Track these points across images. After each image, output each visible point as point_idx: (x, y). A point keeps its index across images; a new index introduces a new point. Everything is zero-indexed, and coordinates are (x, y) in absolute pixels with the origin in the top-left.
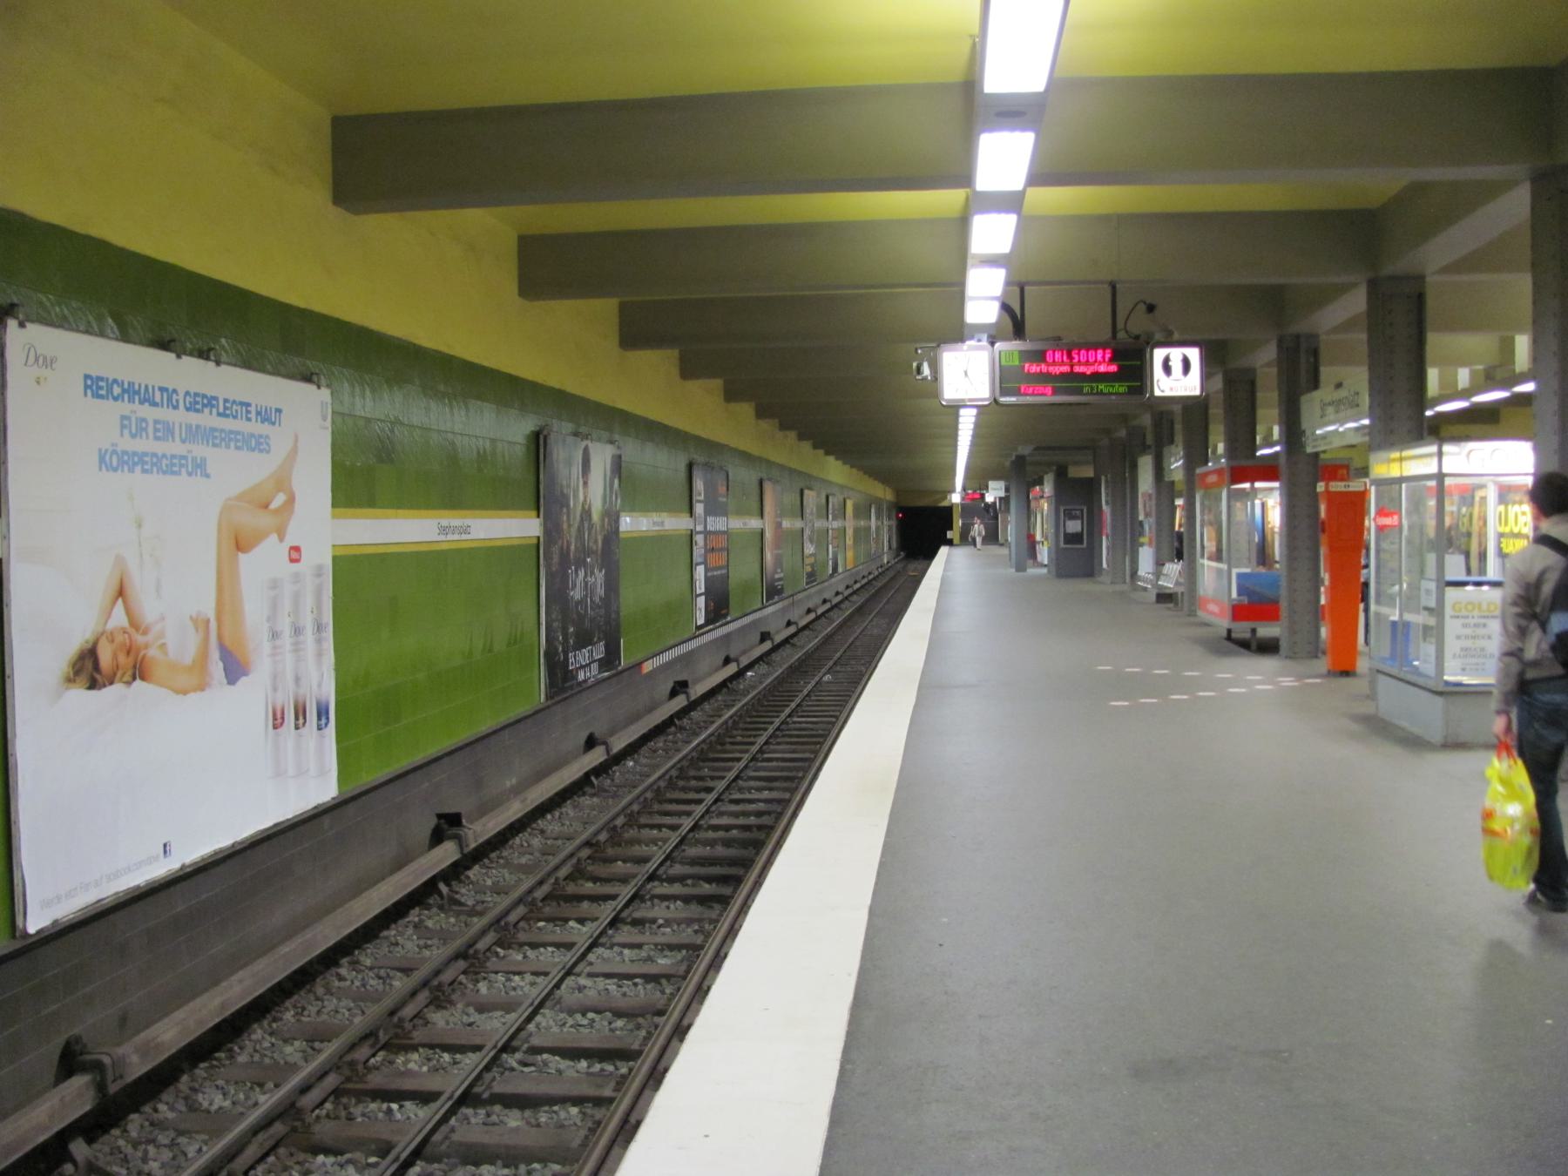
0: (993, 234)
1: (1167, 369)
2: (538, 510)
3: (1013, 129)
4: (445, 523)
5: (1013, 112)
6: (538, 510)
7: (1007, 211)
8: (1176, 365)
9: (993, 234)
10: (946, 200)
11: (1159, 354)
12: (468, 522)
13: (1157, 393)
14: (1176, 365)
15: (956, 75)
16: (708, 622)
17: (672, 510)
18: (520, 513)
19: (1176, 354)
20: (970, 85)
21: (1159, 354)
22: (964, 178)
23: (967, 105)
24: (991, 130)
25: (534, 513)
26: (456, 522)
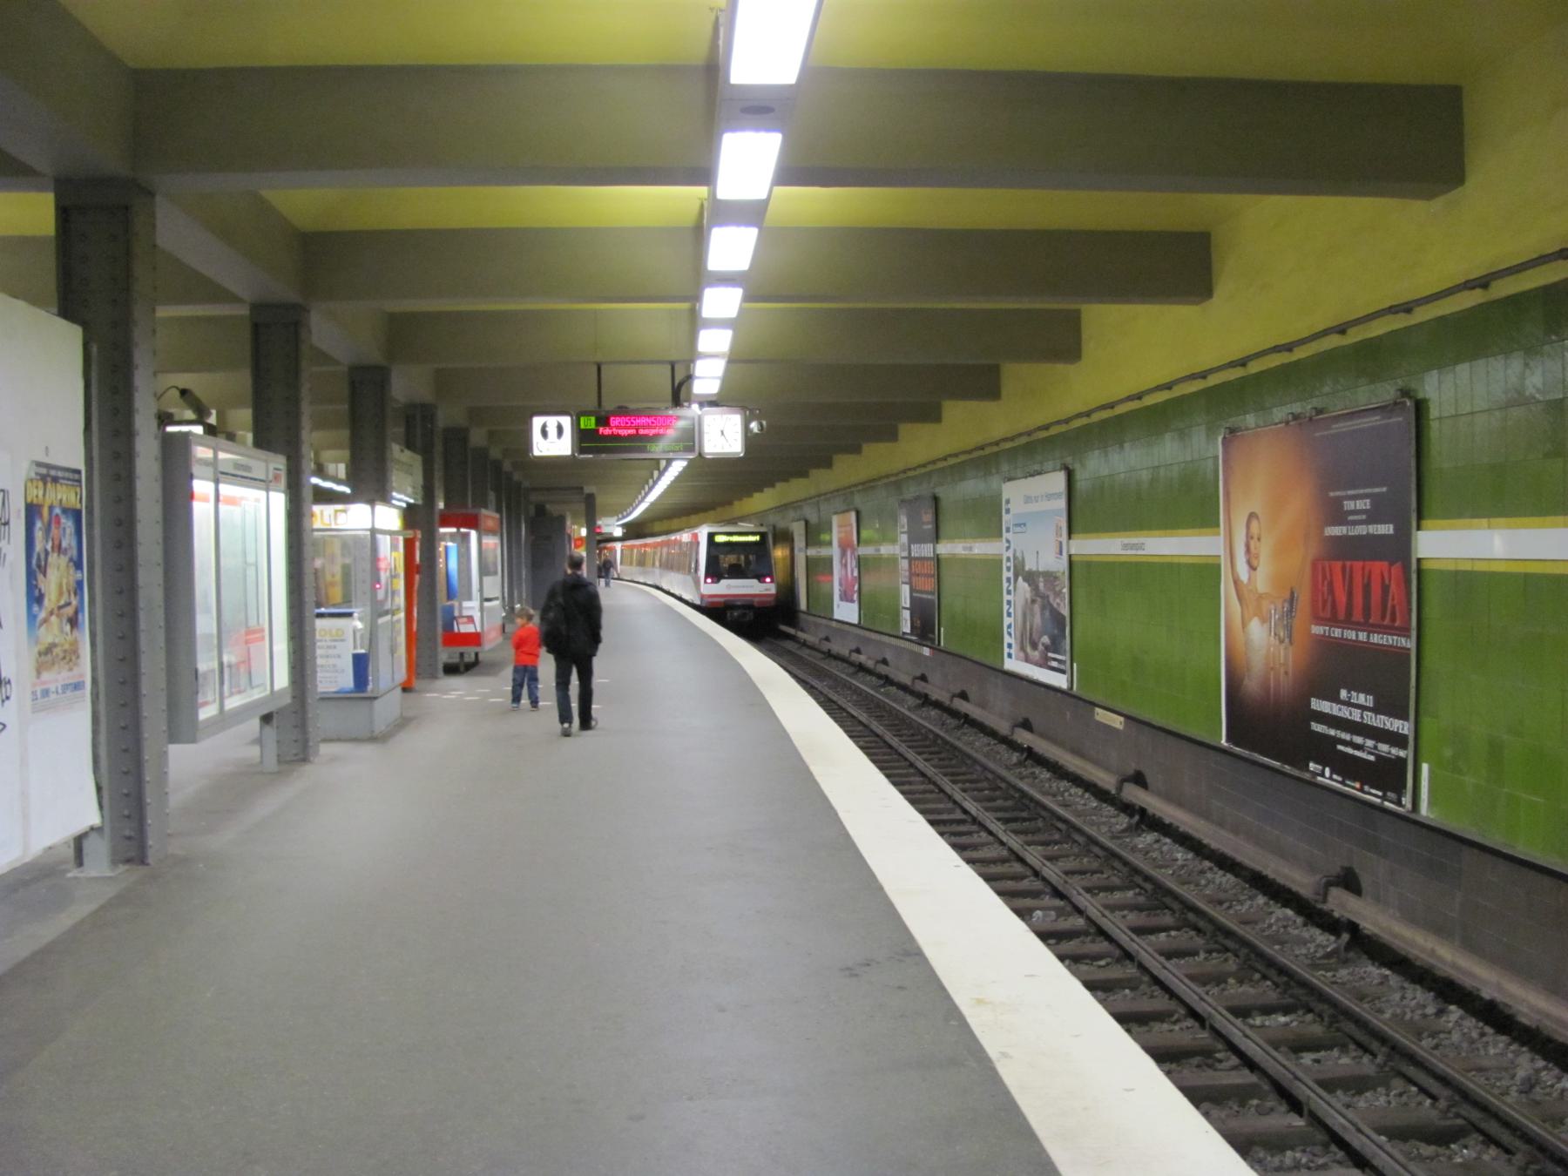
0: (732, 248)
1: (544, 433)
2: (1419, 572)
3: (757, 129)
4: (1126, 541)
5: (760, 108)
6: (1419, 572)
7: (748, 224)
8: (552, 431)
9: (732, 248)
10: (677, 199)
11: (537, 422)
12: (1142, 540)
13: (536, 453)
14: (552, 431)
15: (697, 53)
16: (1267, 937)
17: (954, 559)
18: (1157, 532)
19: (552, 422)
20: (713, 68)
21: (537, 422)
22: (703, 174)
23: (703, 93)
24: (734, 130)
25: (1426, 566)
26: (1134, 540)
